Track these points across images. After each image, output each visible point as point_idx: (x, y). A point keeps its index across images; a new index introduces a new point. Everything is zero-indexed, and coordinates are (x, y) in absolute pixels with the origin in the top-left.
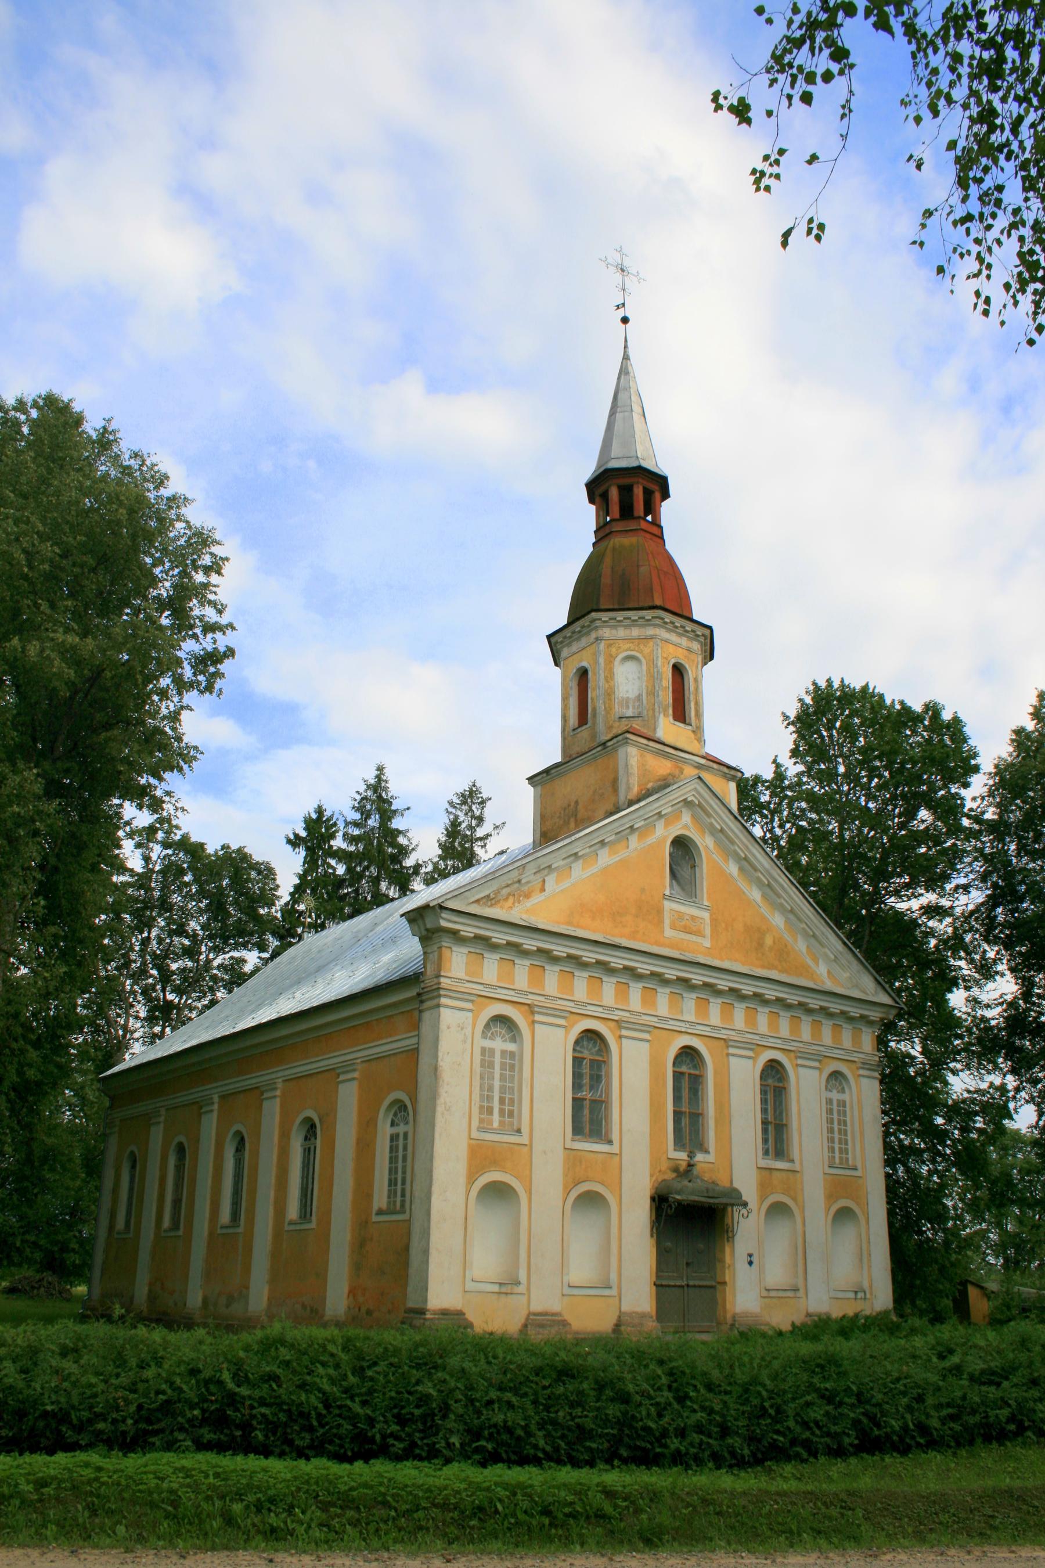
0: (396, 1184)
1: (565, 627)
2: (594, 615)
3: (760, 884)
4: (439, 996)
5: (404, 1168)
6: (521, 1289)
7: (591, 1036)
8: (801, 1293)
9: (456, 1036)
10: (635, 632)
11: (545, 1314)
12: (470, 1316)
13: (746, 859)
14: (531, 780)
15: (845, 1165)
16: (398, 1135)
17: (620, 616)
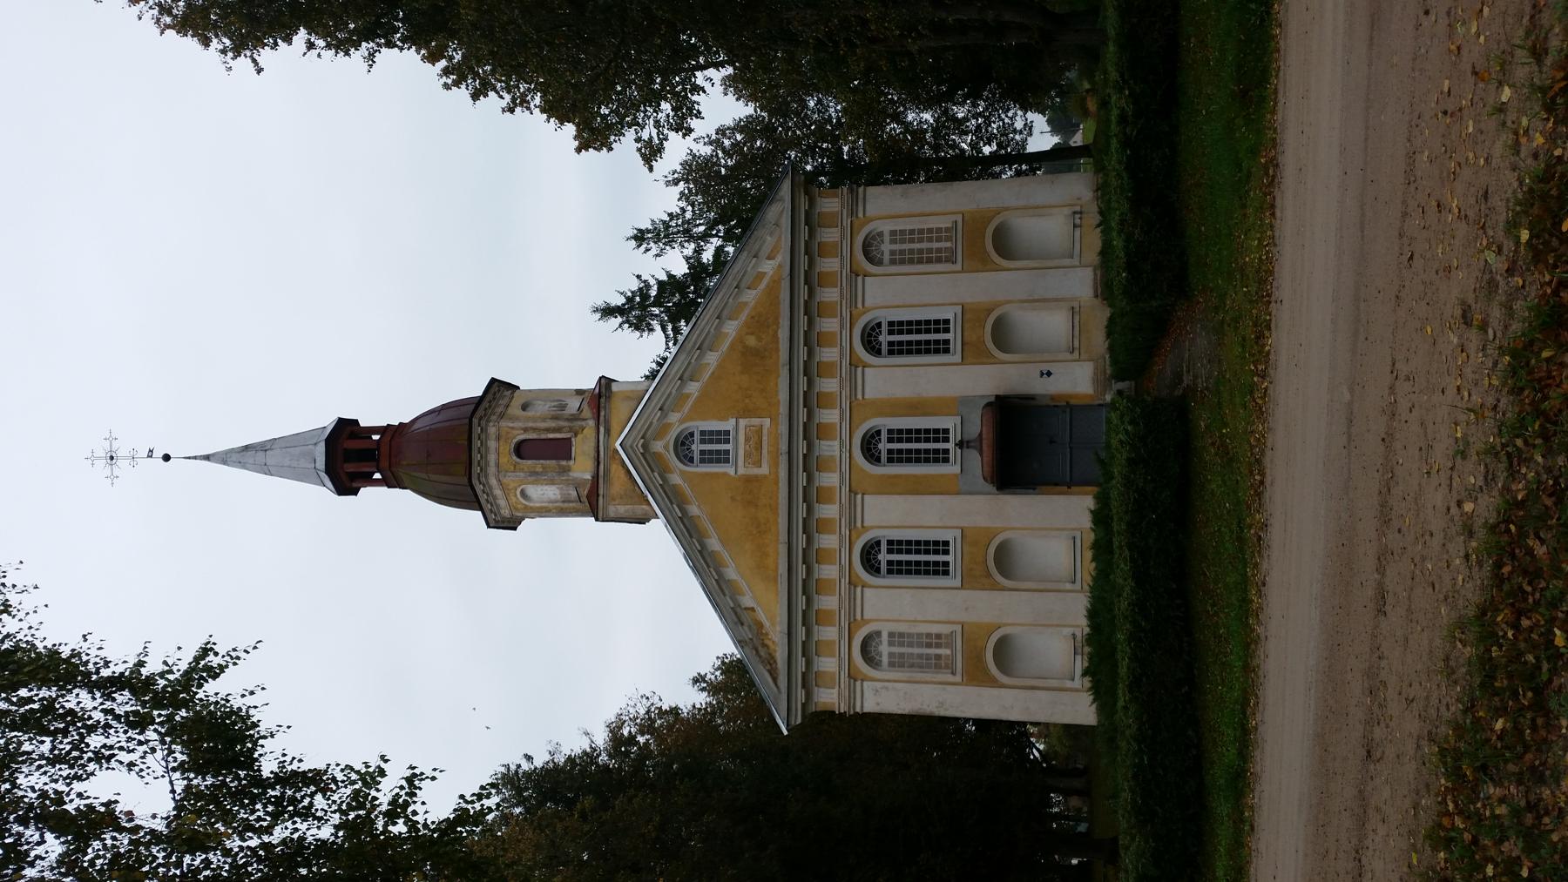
7: (869, 557)
8: (1076, 305)
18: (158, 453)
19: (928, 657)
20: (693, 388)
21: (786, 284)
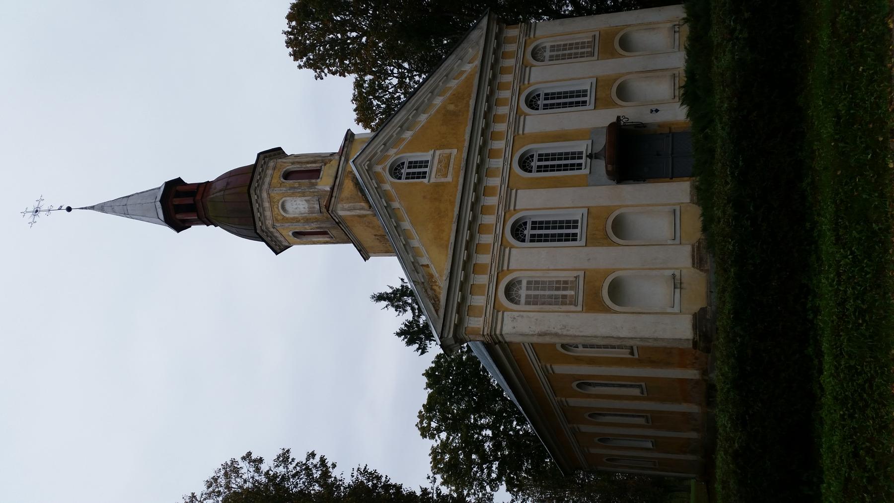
3: (416, 116)
6: (677, 273)
7: (518, 231)
8: (676, 72)
10: (266, 204)
12: (696, 308)
13: (401, 127)
15: (591, 44)
18: (64, 207)
19: (556, 297)
20: (408, 135)
21: (477, 76)
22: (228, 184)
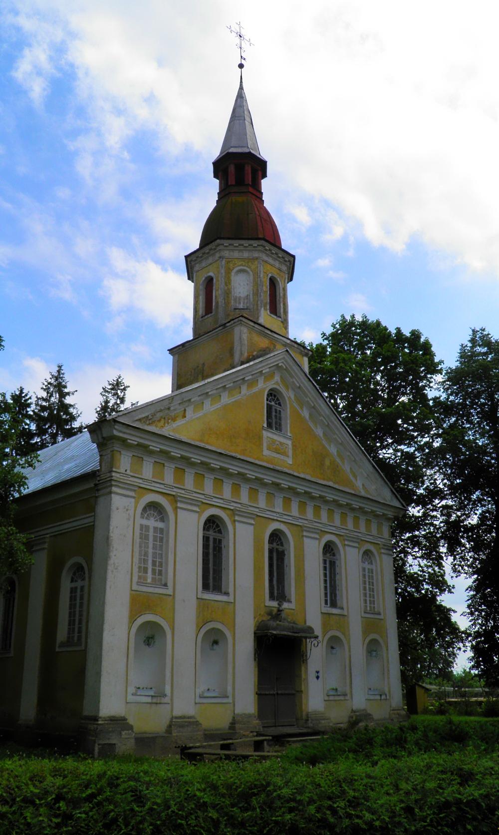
0: (74, 625)
1: (198, 250)
2: (218, 241)
4: (111, 486)
5: (81, 612)
6: (167, 700)
8: (348, 697)
9: (122, 519)
10: (246, 255)
11: (184, 717)
13: (314, 407)
14: (171, 351)
16: (76, 588)
17: (236, 243)
18: (243, 62)
20: (306, 414)
22: (265, 220)
